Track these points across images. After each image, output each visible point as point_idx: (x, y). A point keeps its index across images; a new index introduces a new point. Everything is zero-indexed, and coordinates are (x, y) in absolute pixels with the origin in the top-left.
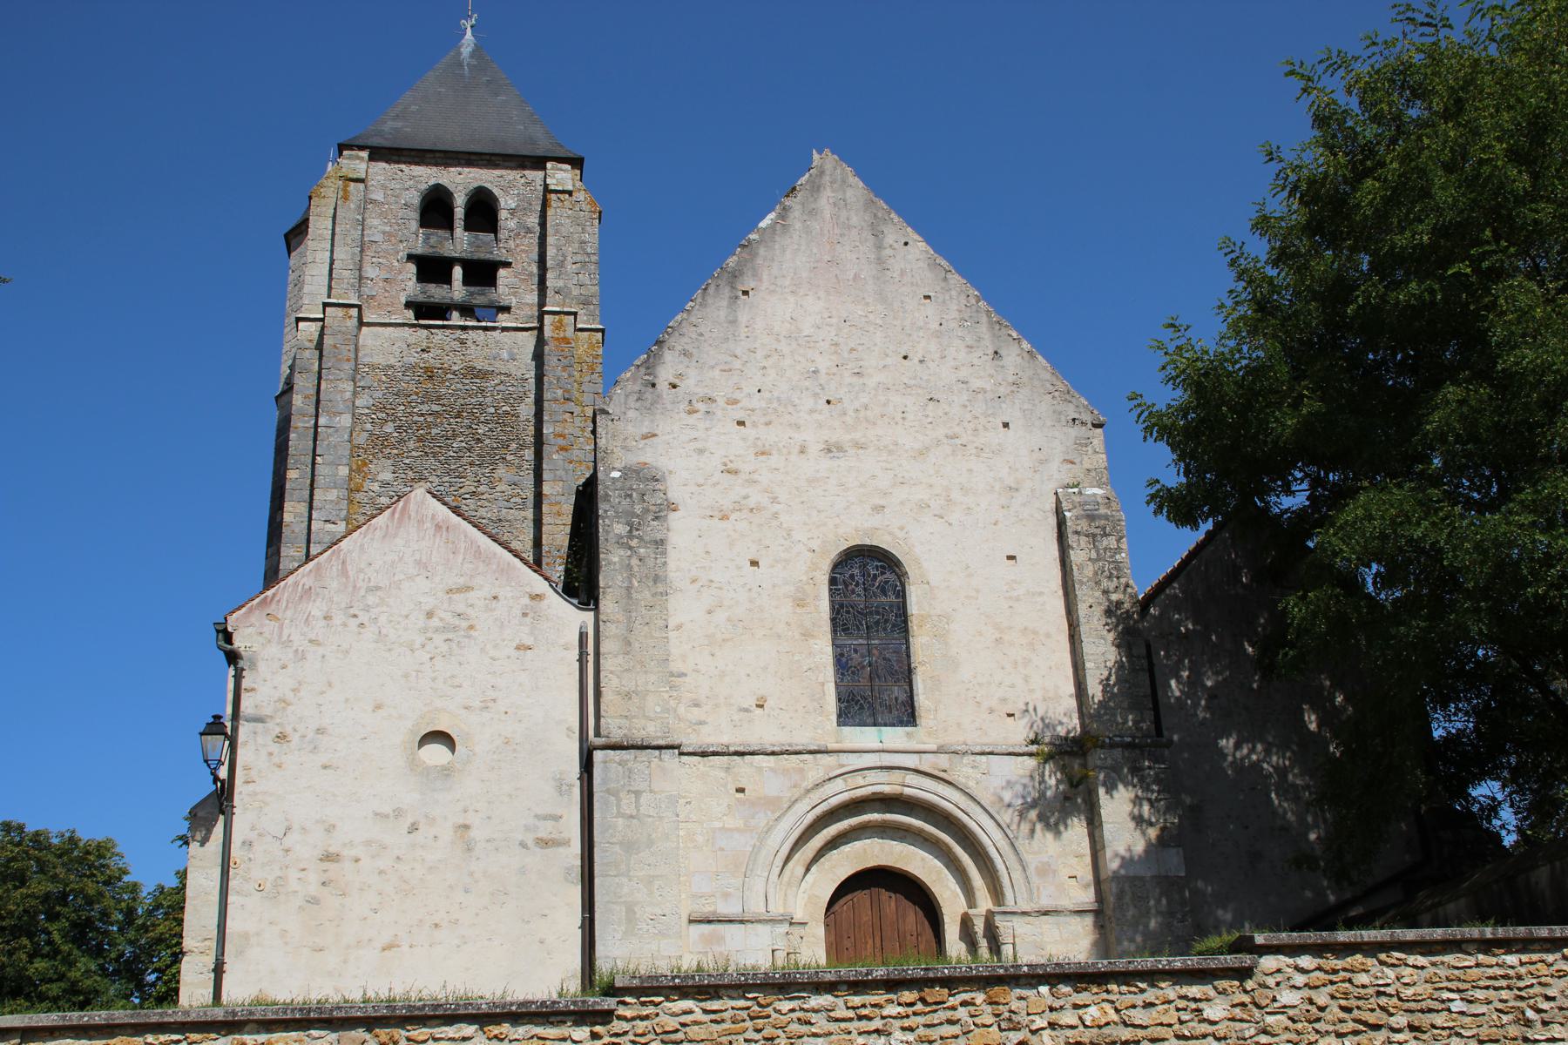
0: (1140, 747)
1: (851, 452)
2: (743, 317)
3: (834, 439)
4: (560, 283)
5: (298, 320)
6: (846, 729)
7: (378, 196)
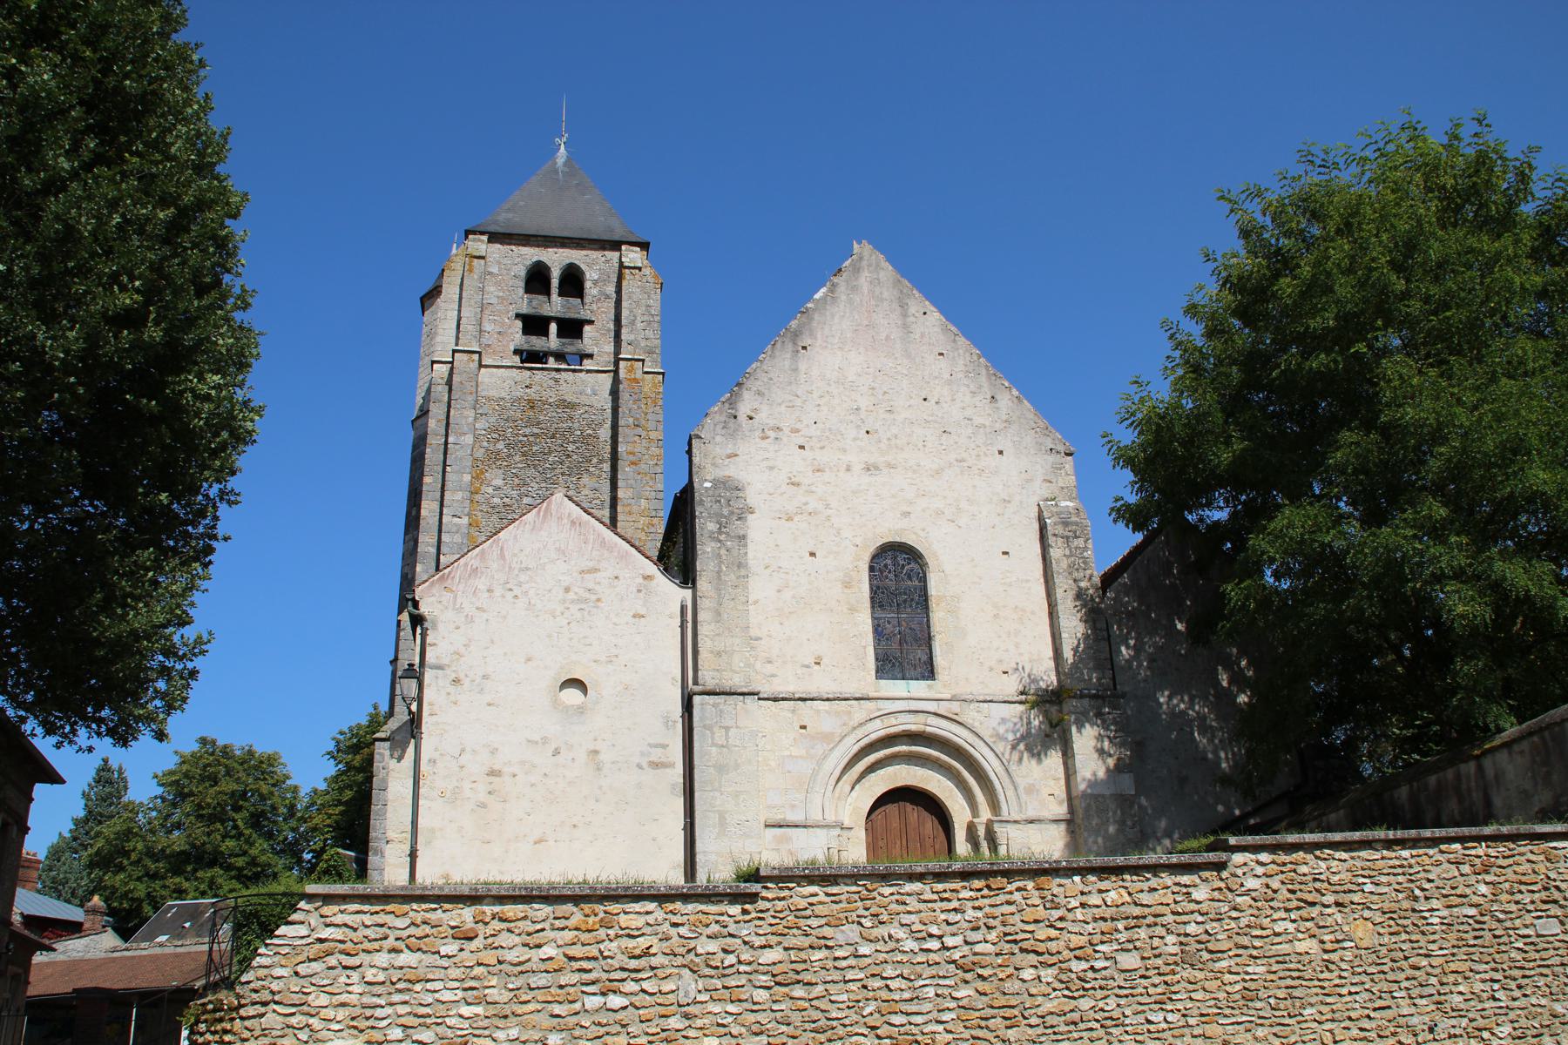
0: (1103, 698)
1: (885, 471)
2: (802, 366)
3: (872, 461)
4: (632, 337)
5: (433, 362)
6: (883, 682)
7: (495, 270)
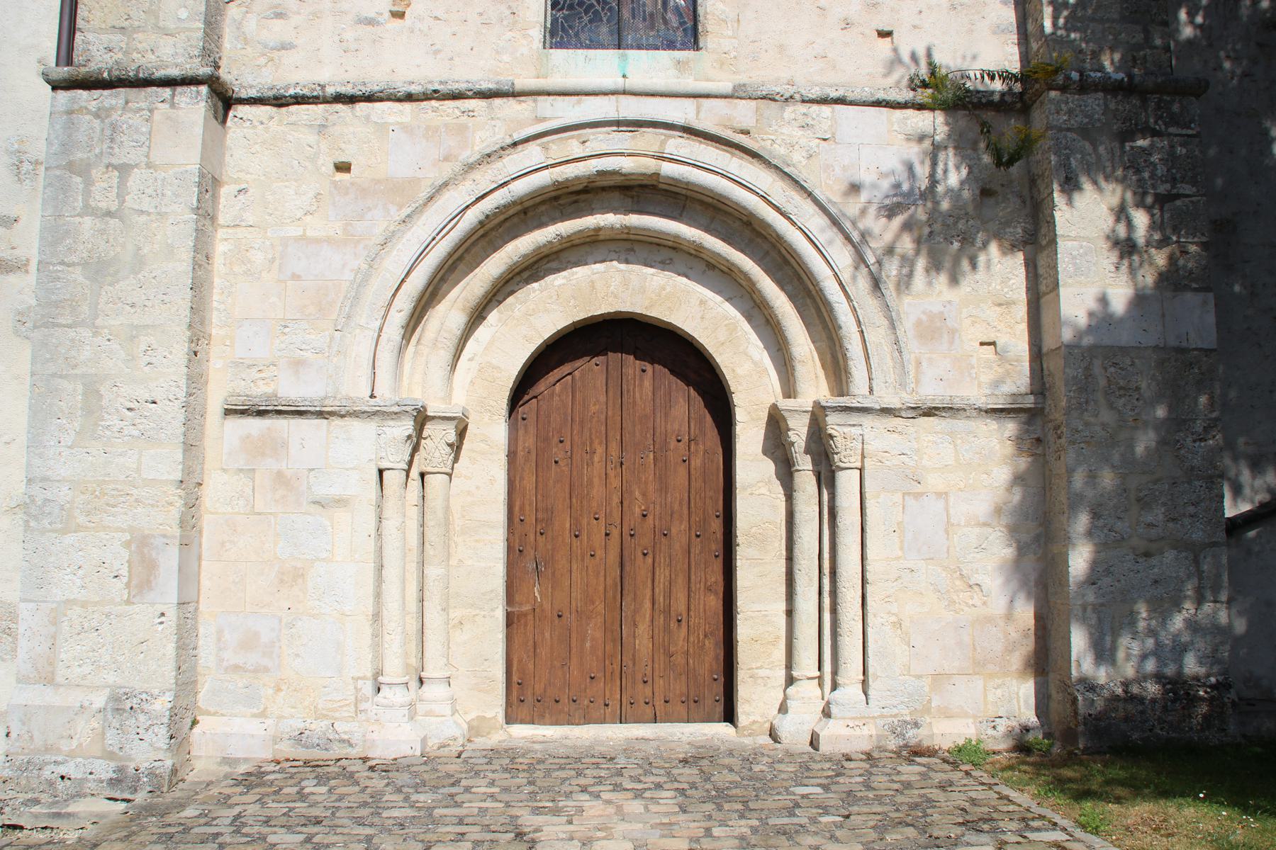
6: (559, 54)
